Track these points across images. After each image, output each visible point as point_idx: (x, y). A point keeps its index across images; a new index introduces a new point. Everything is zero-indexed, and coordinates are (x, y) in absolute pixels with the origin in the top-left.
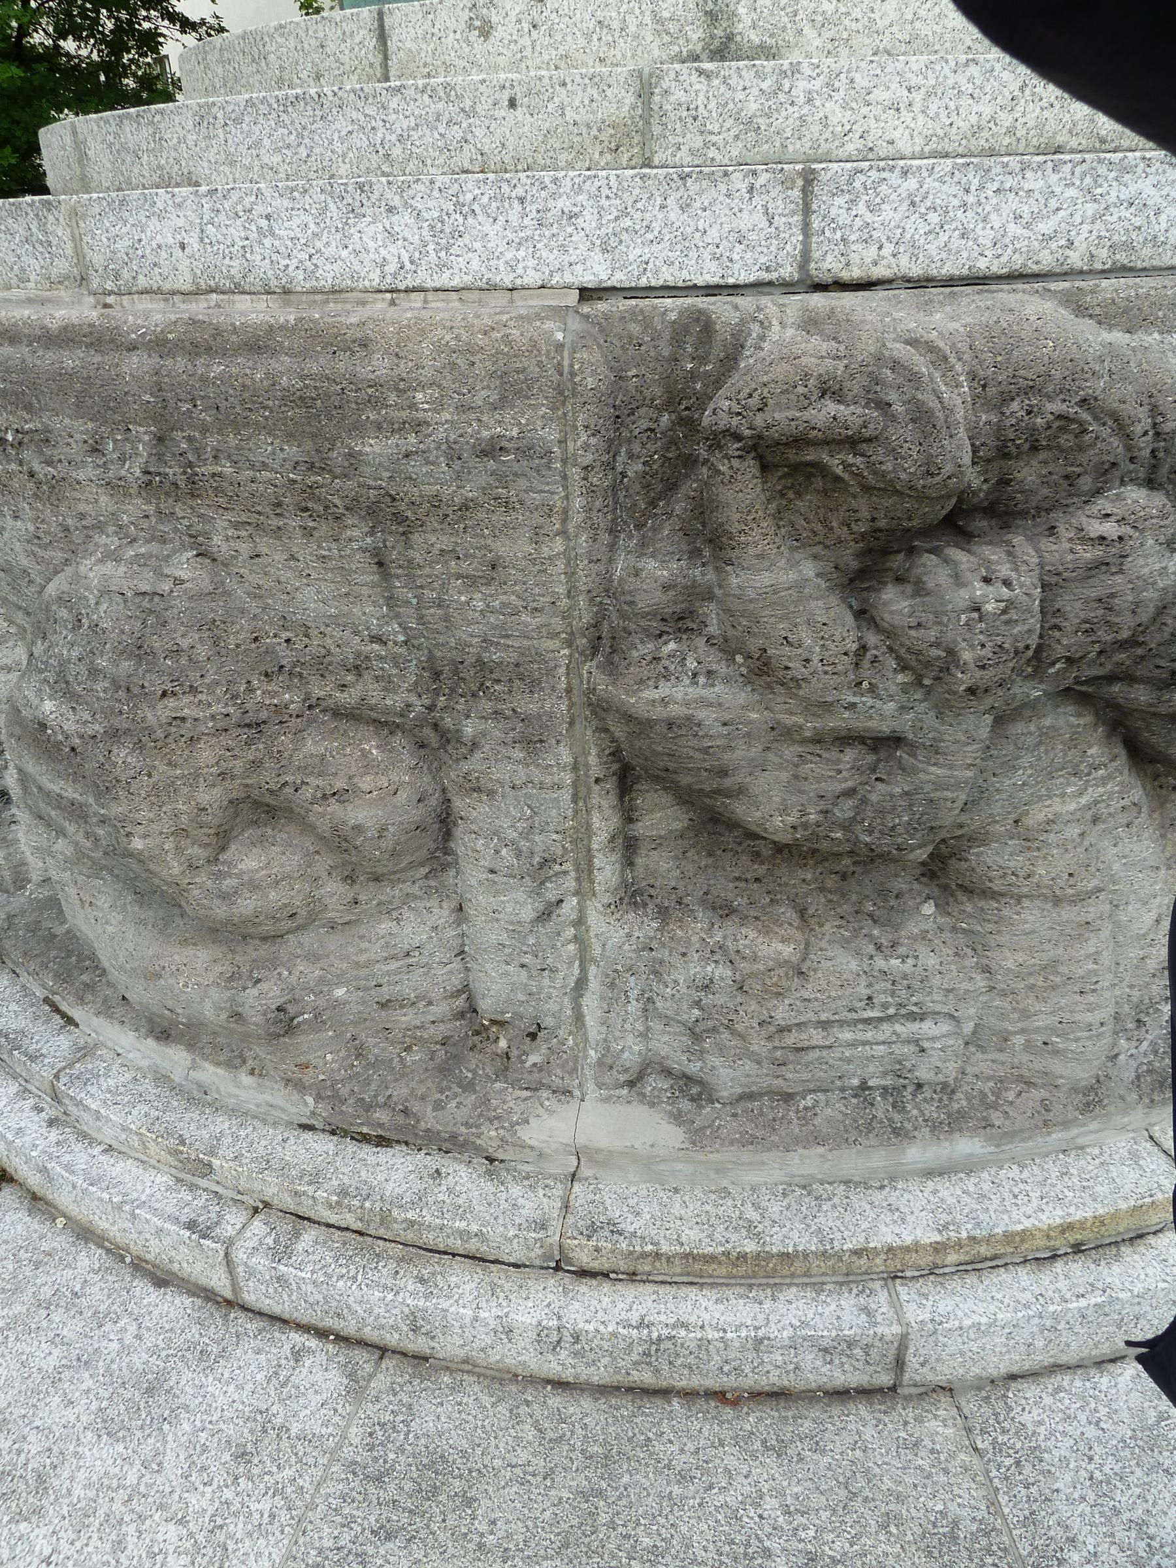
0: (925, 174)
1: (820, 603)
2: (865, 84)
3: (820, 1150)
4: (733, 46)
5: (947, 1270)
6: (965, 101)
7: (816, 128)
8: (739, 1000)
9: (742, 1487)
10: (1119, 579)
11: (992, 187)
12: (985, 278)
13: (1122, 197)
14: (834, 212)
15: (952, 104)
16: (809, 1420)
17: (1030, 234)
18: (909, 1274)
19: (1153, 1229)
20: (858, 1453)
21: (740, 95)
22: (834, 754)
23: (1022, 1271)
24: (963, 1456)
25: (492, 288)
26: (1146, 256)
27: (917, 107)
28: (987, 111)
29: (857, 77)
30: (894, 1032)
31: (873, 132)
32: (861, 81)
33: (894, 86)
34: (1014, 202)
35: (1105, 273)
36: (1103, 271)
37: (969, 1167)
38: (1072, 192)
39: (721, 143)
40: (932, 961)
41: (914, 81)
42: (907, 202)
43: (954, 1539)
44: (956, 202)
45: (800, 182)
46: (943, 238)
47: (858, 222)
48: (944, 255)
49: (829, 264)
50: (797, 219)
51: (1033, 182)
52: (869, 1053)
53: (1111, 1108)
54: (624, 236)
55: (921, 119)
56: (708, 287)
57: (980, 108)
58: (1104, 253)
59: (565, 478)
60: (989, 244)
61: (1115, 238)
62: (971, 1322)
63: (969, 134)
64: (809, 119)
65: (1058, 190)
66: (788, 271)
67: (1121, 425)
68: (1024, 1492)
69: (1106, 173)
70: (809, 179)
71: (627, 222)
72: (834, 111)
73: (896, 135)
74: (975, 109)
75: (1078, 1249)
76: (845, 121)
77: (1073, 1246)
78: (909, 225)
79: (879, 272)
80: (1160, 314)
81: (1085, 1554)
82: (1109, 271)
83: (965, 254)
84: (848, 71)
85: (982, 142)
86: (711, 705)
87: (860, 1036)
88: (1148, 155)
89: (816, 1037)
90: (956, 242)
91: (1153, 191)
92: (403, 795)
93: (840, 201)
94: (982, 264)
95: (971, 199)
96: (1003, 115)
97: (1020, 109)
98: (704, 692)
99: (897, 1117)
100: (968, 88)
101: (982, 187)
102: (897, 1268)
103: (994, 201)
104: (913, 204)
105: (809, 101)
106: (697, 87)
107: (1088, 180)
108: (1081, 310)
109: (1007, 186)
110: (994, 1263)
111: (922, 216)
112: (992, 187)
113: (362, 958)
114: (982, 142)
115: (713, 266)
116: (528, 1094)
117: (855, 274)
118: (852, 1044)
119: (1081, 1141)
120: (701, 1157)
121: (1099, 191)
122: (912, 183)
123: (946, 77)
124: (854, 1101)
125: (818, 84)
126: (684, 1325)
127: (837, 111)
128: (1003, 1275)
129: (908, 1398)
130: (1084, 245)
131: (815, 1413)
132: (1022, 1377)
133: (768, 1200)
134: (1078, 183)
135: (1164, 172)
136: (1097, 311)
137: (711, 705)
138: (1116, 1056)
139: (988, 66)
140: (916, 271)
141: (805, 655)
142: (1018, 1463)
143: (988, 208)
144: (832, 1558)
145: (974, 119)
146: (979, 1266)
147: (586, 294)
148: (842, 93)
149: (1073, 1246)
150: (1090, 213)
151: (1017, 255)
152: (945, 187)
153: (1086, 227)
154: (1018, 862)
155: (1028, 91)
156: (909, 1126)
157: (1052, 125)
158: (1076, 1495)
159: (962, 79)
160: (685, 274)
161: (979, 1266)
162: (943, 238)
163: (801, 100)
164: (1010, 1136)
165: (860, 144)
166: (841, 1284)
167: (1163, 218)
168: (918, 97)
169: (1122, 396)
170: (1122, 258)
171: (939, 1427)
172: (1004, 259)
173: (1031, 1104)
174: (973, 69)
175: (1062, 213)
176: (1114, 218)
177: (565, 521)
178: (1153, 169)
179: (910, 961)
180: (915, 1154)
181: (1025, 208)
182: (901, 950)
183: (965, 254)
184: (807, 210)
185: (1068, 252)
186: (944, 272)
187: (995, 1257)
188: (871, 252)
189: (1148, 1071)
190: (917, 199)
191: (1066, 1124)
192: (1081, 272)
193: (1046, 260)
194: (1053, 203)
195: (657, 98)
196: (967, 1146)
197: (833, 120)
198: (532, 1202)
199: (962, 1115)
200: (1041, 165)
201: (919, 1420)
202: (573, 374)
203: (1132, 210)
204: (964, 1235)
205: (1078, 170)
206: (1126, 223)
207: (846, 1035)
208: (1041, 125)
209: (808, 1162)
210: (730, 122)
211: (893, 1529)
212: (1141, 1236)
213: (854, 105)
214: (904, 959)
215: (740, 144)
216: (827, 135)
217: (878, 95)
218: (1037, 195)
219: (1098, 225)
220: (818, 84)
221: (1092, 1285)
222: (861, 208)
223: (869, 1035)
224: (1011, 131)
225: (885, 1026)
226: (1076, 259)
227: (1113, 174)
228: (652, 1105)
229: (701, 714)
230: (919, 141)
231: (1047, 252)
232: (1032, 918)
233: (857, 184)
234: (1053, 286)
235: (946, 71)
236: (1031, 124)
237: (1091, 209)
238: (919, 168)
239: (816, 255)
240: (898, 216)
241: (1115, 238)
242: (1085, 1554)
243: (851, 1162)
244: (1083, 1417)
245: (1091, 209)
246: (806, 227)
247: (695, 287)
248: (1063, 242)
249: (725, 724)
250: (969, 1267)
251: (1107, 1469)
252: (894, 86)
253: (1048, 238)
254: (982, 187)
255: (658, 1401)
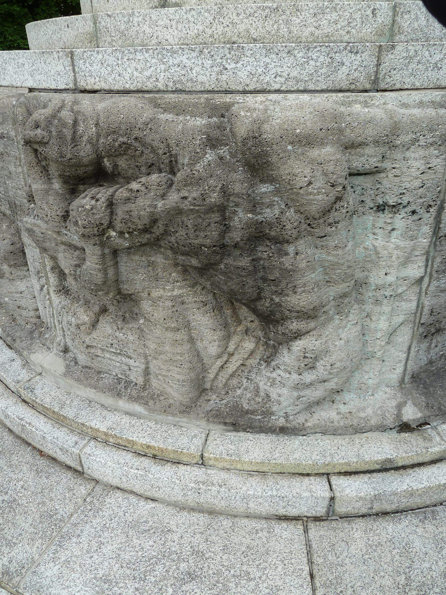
0: (104, 53)
1: (53, 197)
2: (155, 19)
3: (94, 391)
4: (167, 4)
5: (110, 444)
6: (192, 25)
7: (142, 35)
8: (78, 332)
9: (20, 475)
10: (133, 205)
11: (126, 58)
12: (130, 91)
13: (175, 63)
14: (81, 66)
15: (187, 26)
16: (54, 469)
17: (142, 76)
18: (99, 440)
19: (185, 463)
20: (56, 484)
21: (119, 23)
22: (72, 251)
23: (130, 455)
24: (79, 500)
25: (13, 87)
26: (189, 86)
27: (174, 27)
28: (201, 28)
29: (152, 16)
30: (121, 360)
31: (160, 36)
32: (154, 17)
33: (165, 19)
34: (134, 64)
35: (173, 92)
36: (172, 91)
37: (139, 417)
38: (154, 61)
39: (116, 40)
40: (131, 338)
41: (171, 17)
42: (100, 63)
43: (51, 516)
44: (115, 63)
45: (70, 55)
46: (113, 76)
47: (88, 70)
48: (114, 82)
49: (82, 84)
50: (71, 68)
51: (139, 56)
52: (114, 364)
53: (192, 416)
54: (34, 72)
55: (176, 31)
56: (54, 90)
57: (198, 27)
58: (171, 84)
59: (18, 148)
60: (129, 79)
61: (175, 78)
62: (103, 463)
63: (195, 37)
64: (139, 31)
65: (149, 60)
66: (71, 86)
67: (154, 151)
68: (83, 517)
69: (166, 53)
70: (72, 53)
71: (34, 67)
72: (146, 28)
73: (168, 37)
74: (196, 27)
75: (154, 457)
76: (150, 32)
77: (153, 455)
78: (102, 71)
79: (96, 87)
80: (190, 109)
81: (78, 541)
82: (175, 91)
83: (121, 82)
84: (149, 14)
85: (201, 40)
86: (38, 226)
87: (111, 357)
88: (182, 47)
89: (99, 353)
90: (118, 78)
91: (187, 61)
92: (6, 241)
93: (81, 62)
94: (127, 86)
95: (120, 62)
96: (207, 30)
97: (214, 27)
98: (36, 222)
99: (123, 390)
100: (192, 19)
101: (122, 58)
102: (95, 437)
103: (127, 63)
104: (102, 63)
105: (139, 25)
106: (108, 20)
107: (160, 56)
108: (157, 106)
109: (131, 58)
110: (125, 448)
111: (106, 68)
112: (126, 58)
113: (10, 290)
114: (201, 40)
115: (53, 82)
116: (42, 346)
117: (89, 87)
118: (110, 359)
119: (181, 424)
120: (65, 379)
121: (165, 60)
122: (100, 56)
123: (183, 15)
124: (116, 381)
125: (140, 19)
126: (30, 424)
127: (148, 28)
128: (124, 453)
129: (84, 478)
130: (163, 81)
131: (58, 469)
132: (121, 490)
133: (77, 402)
134: (156, 57)
135: (190, 53)
136: (164, 106)
137: (38, 226)
138: (209, 400)
139: (199, 11)
140: (107, 88)
141: (46, 214)
142: (91, 510)
143: (126, 66)
144: (19, 503)
145: (196, 31)
146: (120, 447)
147: (31, 90)
148: (148, 22)
149: (153, 455)
150: (163, 69)
151: (138, 84)
152: (111, 58)
153: (162, 74)
154: (149, 309)
155: (216, 21)
156: (123, 394)
157: (229, 34)
158: (95, 526)
159: (189, 16)
160: (48, 85)
161: (120, 447)
162: (113, 76)
163: (136, 25)
164: (154, 411)
165: (156, 41)
166: (79, 433)
167: (194, 71)
168: (174, 23)
169: (152, 138)
170: (179, 86)
171: (82, 490)
172: (134, 85)
173: (166, 403)
174: (193, 12)
175: (152, 68)
176: (173, 71)
177: (20, 162)
178: (185, 52)
179: (126, 336)
180: (122, 404)
181: (139, 66)
182: (123, 331)
183: (121, 82)
184: (73, 65)
185: (157, 83)
186: (115, 88)
187: (125, 446)
188: (93, 81)
189: (218, 410)
190: (103, 62)
191: (173, 415)
192: (164, 91)
193: (149, 86)
194: (148, 65)
195: (98, 24)
196: (138, 408)
197: (147, 32)
198: (24, 375)
199: (142, 398)
200: (141, 50)
201: (80, 485)
202: (17, 115)
203: (180, 68)
204: (113, 433)
205: (155, 52)
206: (178, 73)
207: (107, 355)
208: (224, 34)
209: (90, 393)
210: (118, 32)
211: (40, 506)
212: (178, 463)
213: (152, 26)
214: (124, 334)
215: (121, 40)
216: (146, 37)
217: (160, 23)
218: (142, 61)
219: (167, 73)
220: (140, 19)
221: (145, 468)
222: (87, 65)
223: (114, 358)
224: (212, 36)
225: (120, 357)
226: (160, 86)
227: (169, 54)
228: (65, 360)
229: (35, 229)
230: (177, 40)
231: (149, 83)
232: (158, 332)
233: (85, 56)
234: (147, 96)
235: (183, 13)
236: (220, 33)
237: (163, 67)
238: (102, 51)
239: (78, 80)
240: (98, 68)
241: (175, 78)
242: (78, 541)
243: (109, 401)
244: (123, 509)
245: (163, 67)
246: (74, 71)
247: (51, 89)
248: (154, 79)
249: (42, 234)
250: (117, 446)
251: (112, 525)
252: (165, 19)
253: (149, 78)
254: (122, 58)
255: (26, 445)
